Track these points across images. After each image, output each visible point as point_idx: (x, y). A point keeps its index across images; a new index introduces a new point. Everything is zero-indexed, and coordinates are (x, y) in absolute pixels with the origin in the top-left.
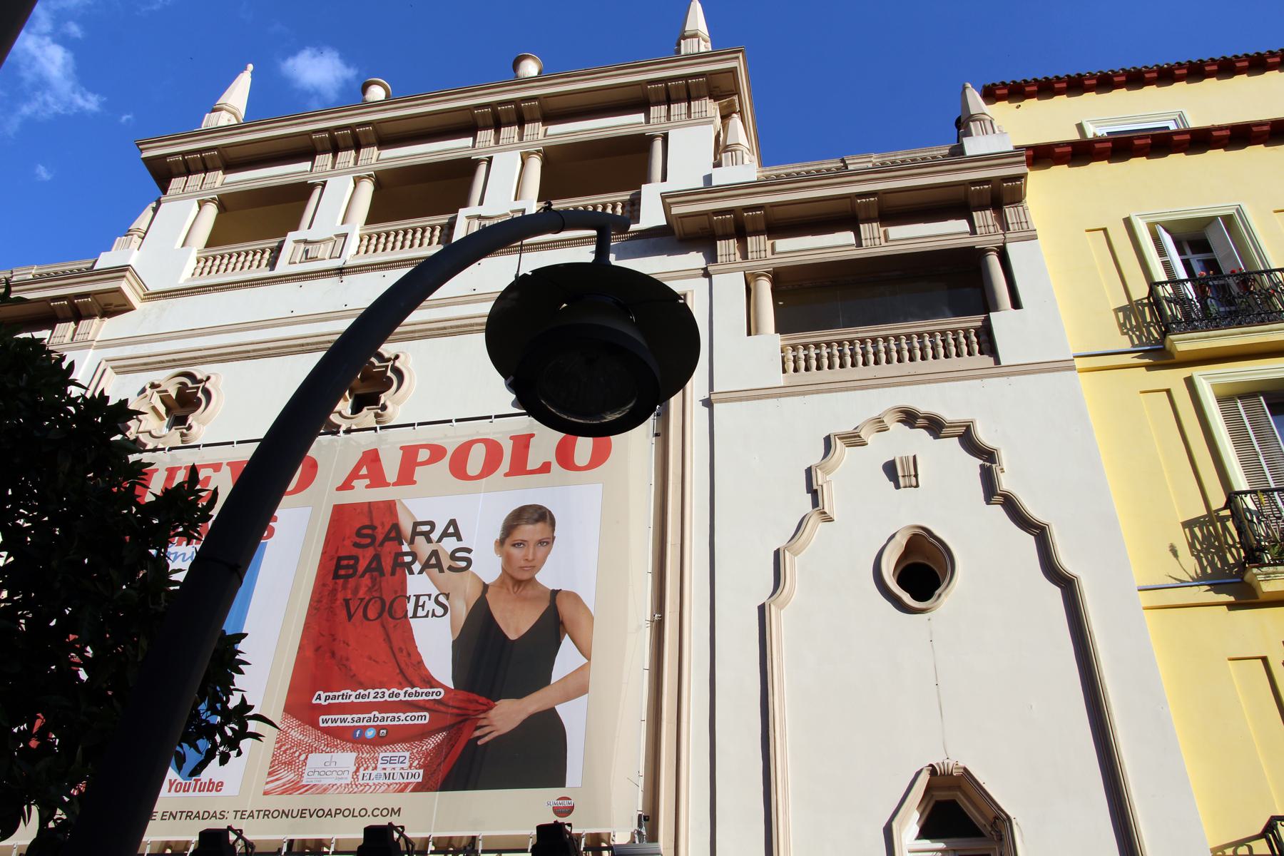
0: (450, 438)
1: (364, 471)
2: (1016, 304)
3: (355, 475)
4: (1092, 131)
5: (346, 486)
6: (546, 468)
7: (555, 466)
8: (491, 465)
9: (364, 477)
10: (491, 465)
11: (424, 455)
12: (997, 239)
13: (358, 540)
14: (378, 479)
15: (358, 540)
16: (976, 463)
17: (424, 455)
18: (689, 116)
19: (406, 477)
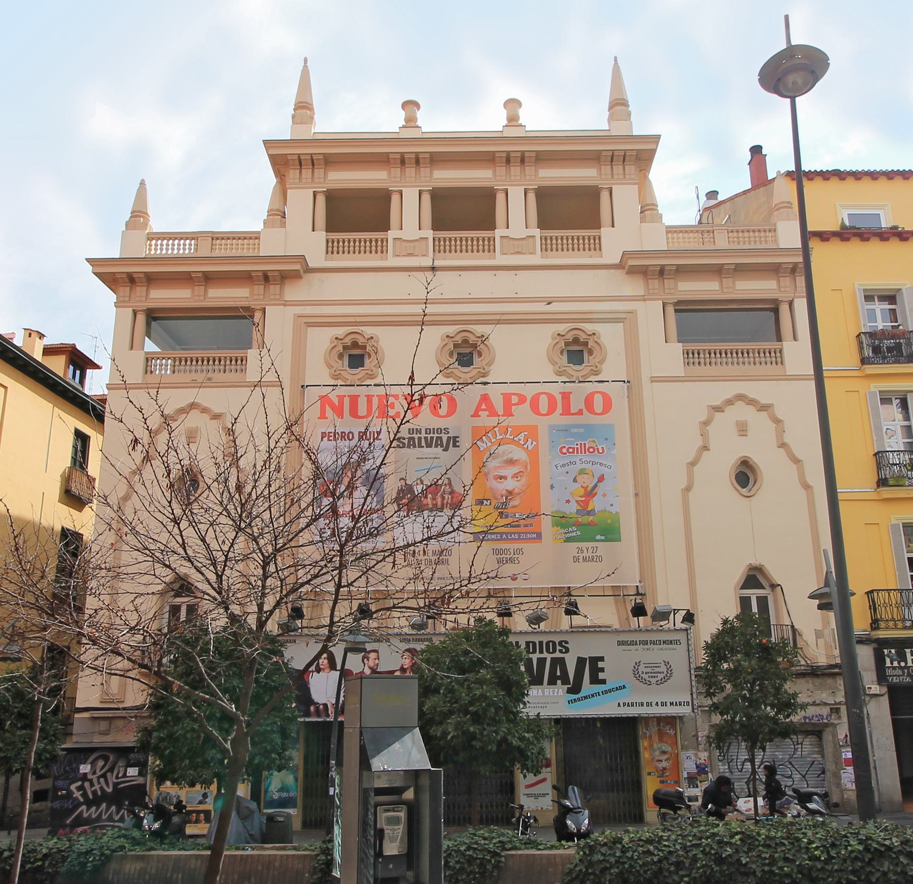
0: (529, 391)
1: (484, 407)
2: (795, 338)
3: (478, 409)
4: (435, 122)
5: (476, 415)
6: (580, 412)
7: (585, 411)
8: (552, 409)
9: (484, 410)
10: (552, 409)
11: (515, 399)
12: (789, 296)
13: (341, 252)
14: (493, 413)
15: (341, 252)
16: (764, 414)
17: (515, 399)
18: (612, 177)
19: (508, 413)
